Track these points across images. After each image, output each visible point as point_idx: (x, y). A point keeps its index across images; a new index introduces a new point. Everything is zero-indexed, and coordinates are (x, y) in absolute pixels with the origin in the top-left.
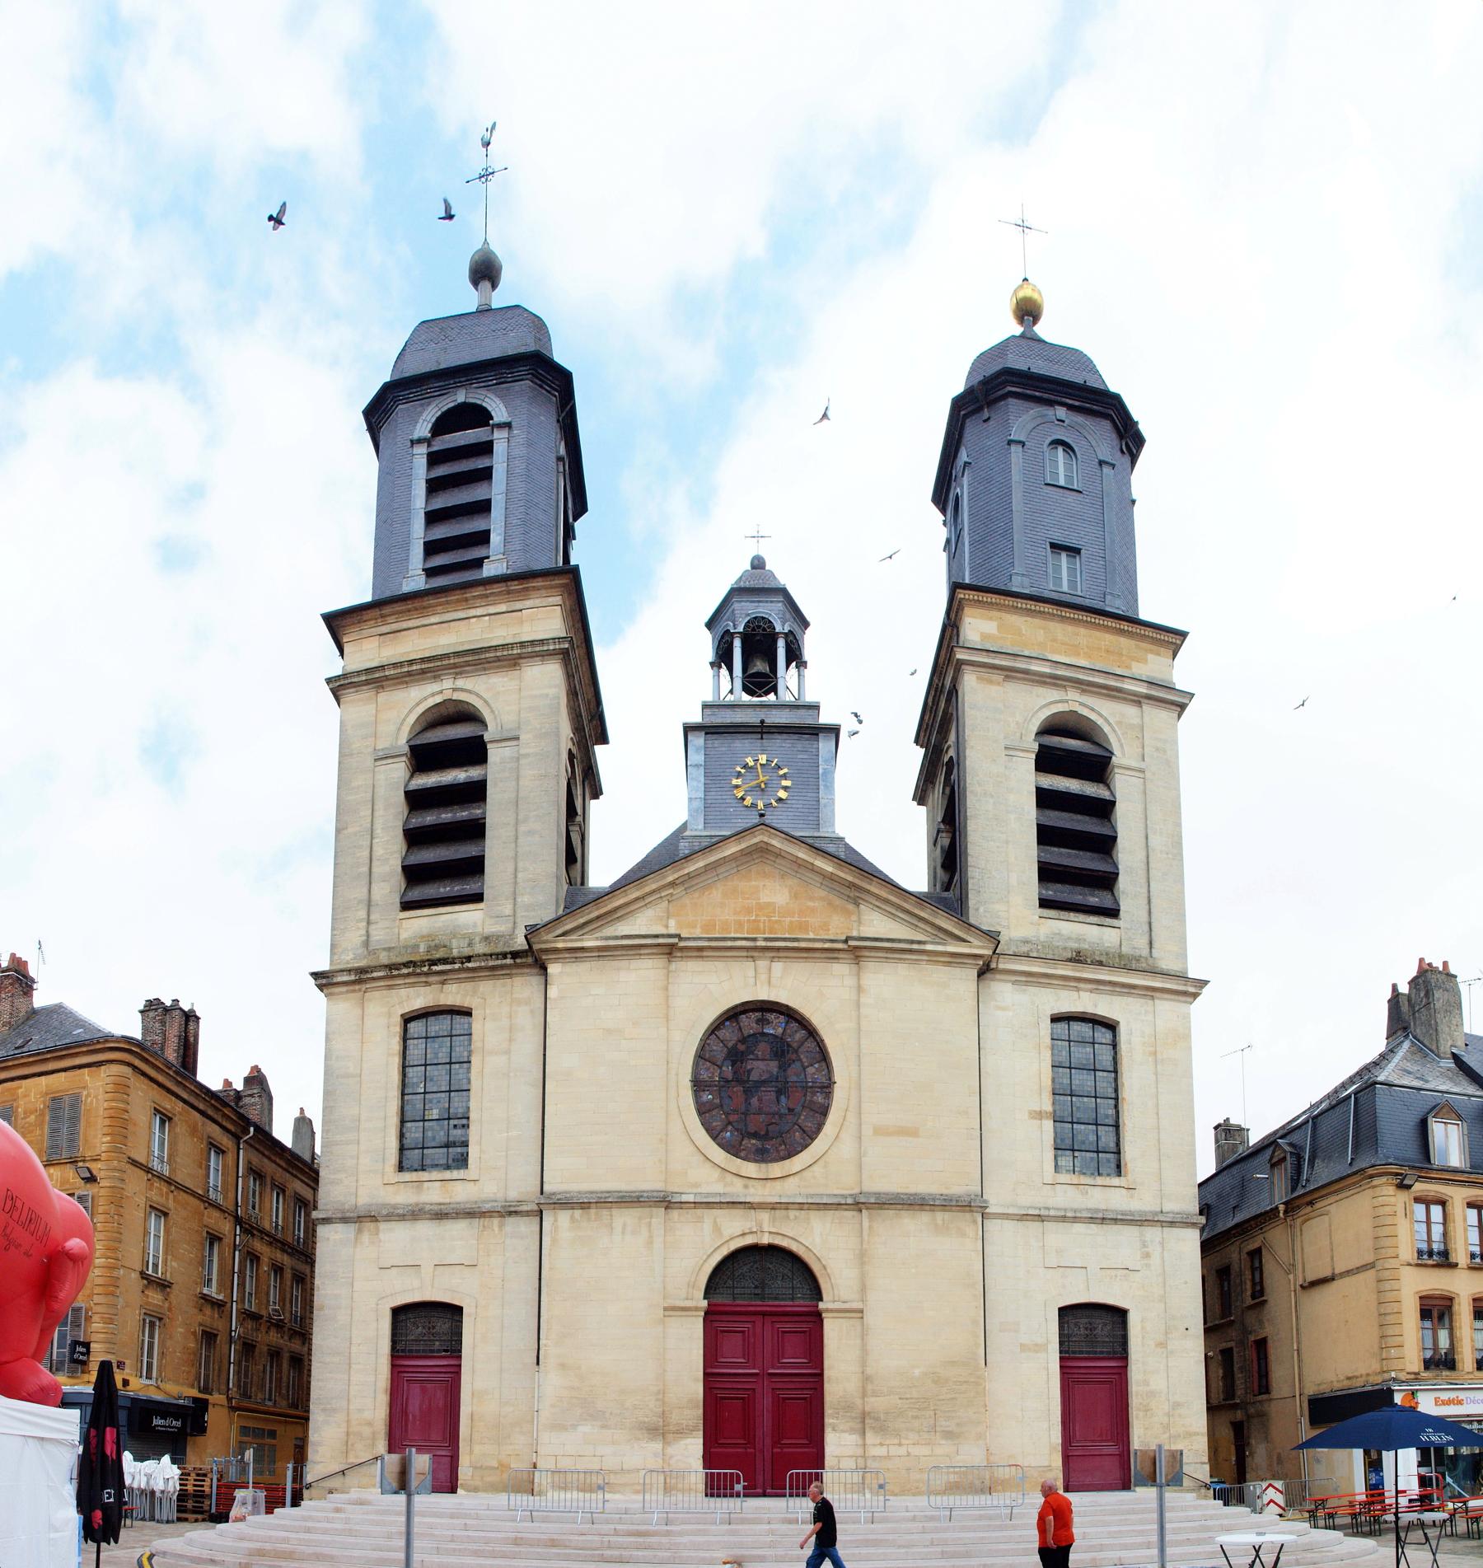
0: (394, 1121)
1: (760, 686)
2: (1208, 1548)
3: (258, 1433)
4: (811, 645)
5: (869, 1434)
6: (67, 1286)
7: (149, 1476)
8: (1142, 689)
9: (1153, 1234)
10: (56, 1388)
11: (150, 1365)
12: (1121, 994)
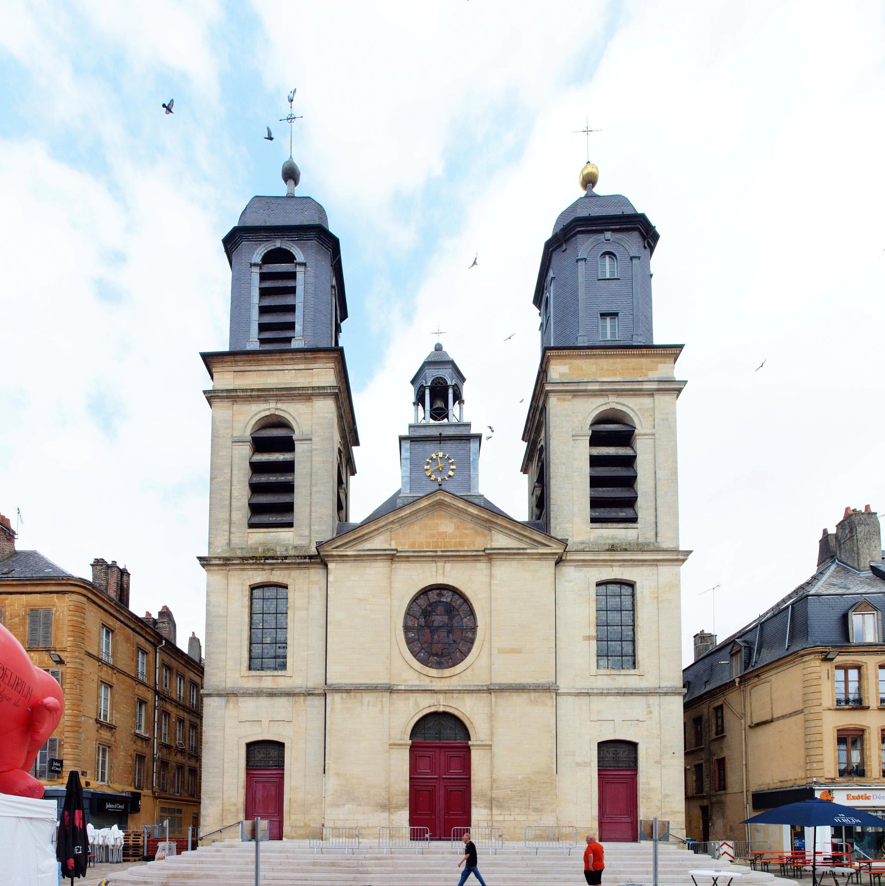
0: (246, 643)
1: (439, 415)
2: (684, 877)
3: (171, 811)
4: (467, 391)
5: (494, 809)
6: (46, 725)
7: (104, 837)
8: (654, 386)
9: (654, 700)
10: (40, 787)
11: (103, 774)
12: (637, 566)
